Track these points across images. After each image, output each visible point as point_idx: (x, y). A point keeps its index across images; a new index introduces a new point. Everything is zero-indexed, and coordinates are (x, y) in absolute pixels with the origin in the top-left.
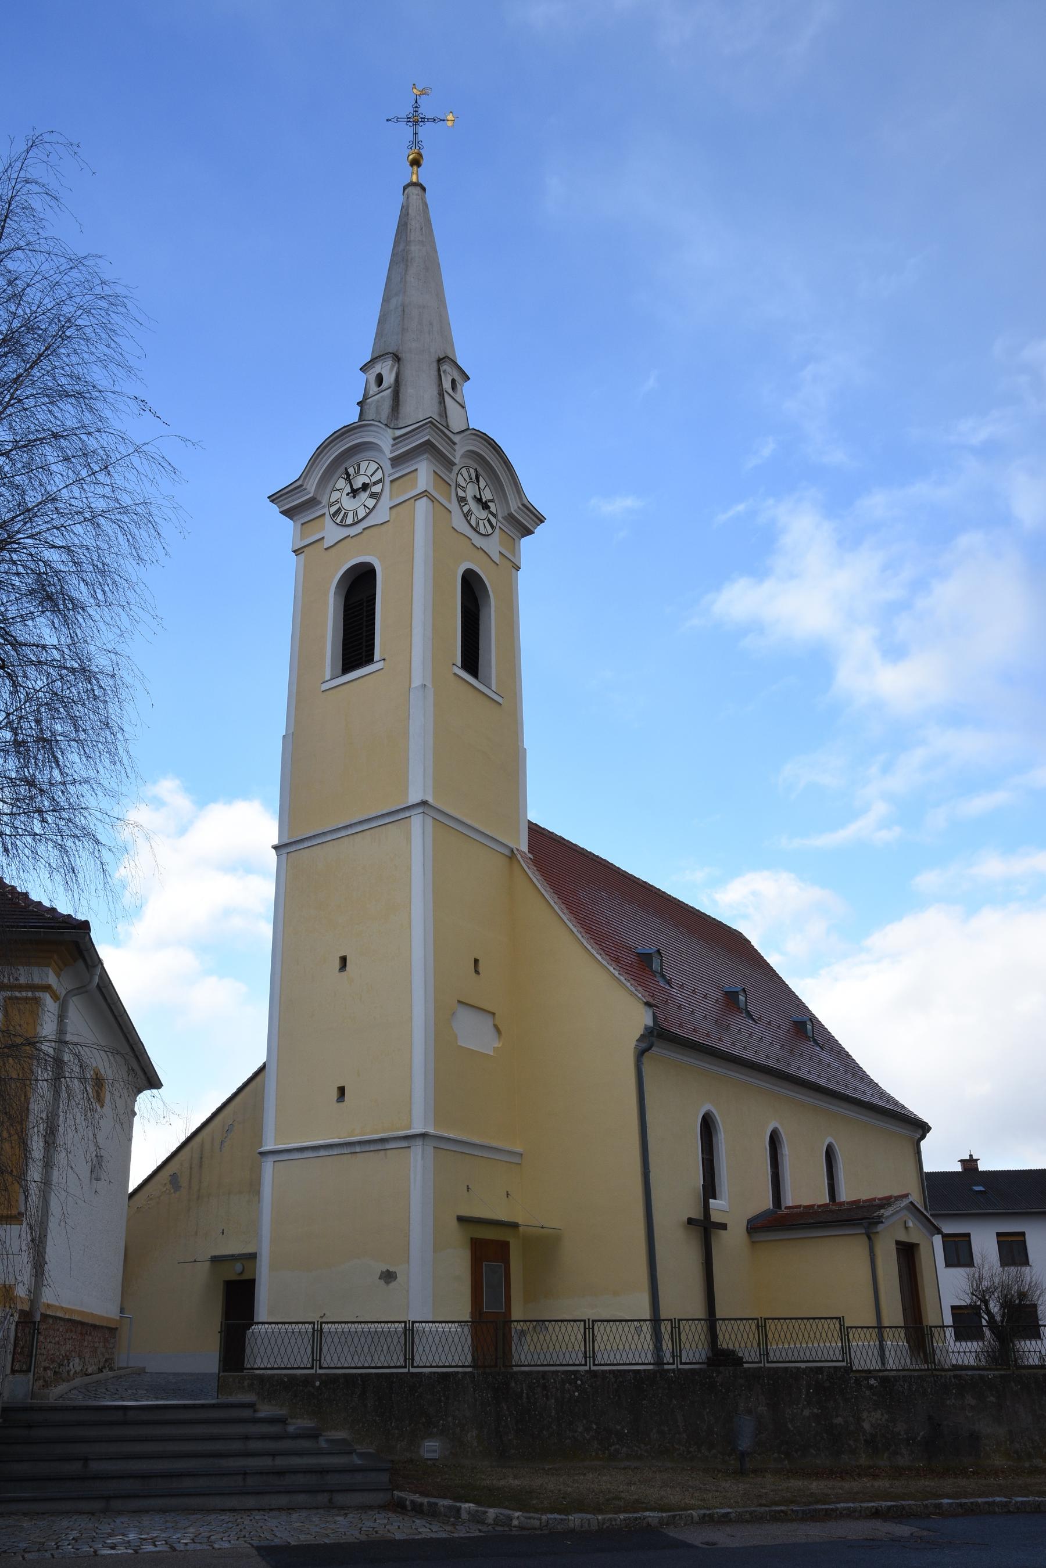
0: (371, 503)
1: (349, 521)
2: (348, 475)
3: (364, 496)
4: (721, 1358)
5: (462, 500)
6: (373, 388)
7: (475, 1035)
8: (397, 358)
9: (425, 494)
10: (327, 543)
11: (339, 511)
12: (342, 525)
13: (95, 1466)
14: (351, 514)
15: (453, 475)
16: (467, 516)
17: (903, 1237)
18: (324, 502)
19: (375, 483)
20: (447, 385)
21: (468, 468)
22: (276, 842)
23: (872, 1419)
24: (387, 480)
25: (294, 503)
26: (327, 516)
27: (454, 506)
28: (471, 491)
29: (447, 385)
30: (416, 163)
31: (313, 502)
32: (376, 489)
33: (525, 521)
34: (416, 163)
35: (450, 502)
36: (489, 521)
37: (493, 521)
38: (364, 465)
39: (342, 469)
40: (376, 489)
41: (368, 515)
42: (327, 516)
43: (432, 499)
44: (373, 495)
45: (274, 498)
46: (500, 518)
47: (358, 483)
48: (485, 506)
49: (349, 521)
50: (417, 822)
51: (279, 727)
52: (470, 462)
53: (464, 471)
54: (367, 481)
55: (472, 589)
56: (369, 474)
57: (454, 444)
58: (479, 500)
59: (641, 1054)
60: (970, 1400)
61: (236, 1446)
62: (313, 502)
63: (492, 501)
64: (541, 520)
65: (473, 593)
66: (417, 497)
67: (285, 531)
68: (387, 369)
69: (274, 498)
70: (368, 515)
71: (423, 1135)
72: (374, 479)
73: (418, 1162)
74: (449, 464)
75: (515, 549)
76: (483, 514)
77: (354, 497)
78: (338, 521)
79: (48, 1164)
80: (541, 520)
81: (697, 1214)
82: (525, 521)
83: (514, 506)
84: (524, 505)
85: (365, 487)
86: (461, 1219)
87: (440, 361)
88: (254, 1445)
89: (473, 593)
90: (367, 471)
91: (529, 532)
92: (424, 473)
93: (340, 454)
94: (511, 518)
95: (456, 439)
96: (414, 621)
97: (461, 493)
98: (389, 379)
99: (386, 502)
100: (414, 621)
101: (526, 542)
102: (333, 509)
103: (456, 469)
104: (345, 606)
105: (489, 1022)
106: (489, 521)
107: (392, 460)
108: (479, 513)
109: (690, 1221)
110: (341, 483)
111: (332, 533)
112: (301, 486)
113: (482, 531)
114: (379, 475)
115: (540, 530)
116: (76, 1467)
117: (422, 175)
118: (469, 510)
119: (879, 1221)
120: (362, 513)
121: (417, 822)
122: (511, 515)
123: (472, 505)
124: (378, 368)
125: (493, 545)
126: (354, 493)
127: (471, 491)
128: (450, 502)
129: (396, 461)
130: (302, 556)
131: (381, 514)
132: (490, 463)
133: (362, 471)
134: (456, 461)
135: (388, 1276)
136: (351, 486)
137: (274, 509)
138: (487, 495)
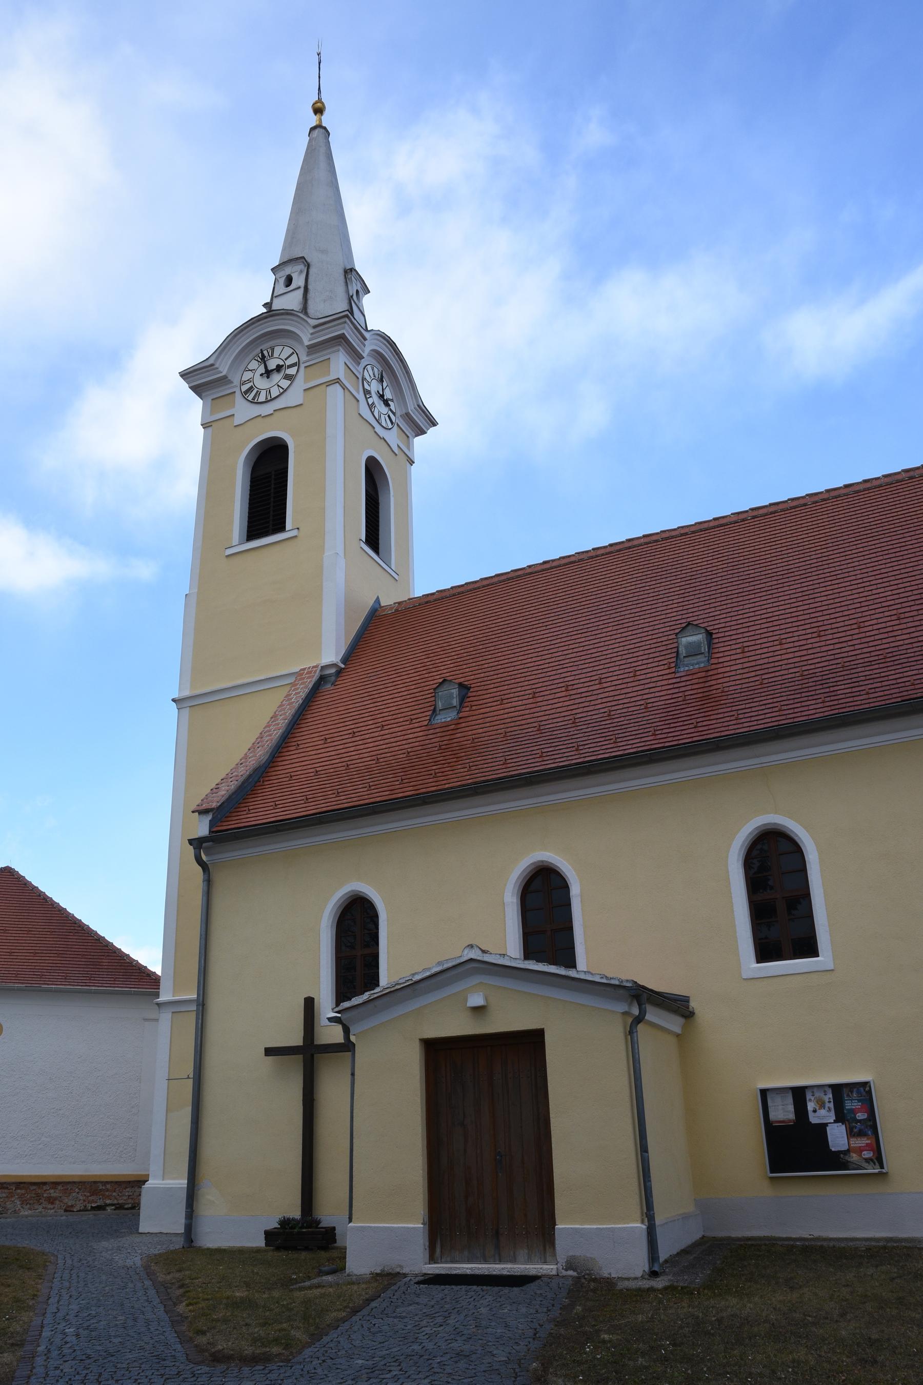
0: (285, 383)
1: (262, 398)
2: (263, 356)
3: (277, 377)
5: (367, 393)
6: (281, 289)
10: (237, 420)
11: (250, 389)
14: (263, 394)
16: (371, 407)
18: (236, 382)
19: (290, 366)
24: (302, 366)
26: (238, 395)
28: (374, 387)
32: (292, 371)
35: (358, 392)
36: (389, 416)
38: (277, 350)
39: (258, 350)
40: (292, 371)
41: (281, 394)
42: (238, 395)
43: (344, 388)
44: (288, 377)
45: (185, 375)
46: (398, 414)
47: (272, 364)
48: (386, 403)
49: (262, 398)
52: (374, 362)
53: (369, 367)
54: (281, 363)
55: (374, 474)
56: (283, 356)
57: (365, 339)
58: (381, 396)
63: (392, 400)
64: (434, 423)
66: (329, 384)
67: (196, 405)
70: (281, 394)
72: (288, 362)
74: (357, 356)
75: (409, 445)
76: (384, 410)
77: (268, 377)
78: (250, 398)
79: (628, 1279)
80: (434, 423)
82: (420, 421)
84: (419, 406)
85: (279, 368)
90: (281, 354)
91: (423, 432)
92: (339, 363)
93: (258, 338)
94: (408, 417)
96: (325, 496)
99: (300, 383)
102: (244, 388)
103: (363, 363)
104: (252, 478)
106: (389, 416)
107: (309, 347)
108: (381, 408)
112: (212, 365)
113: (384, 424)
114: (294, 359)
115: (432, 431)
118: (373, 403)
120: (275, 392)
122: (408, 414)
123: (375, 399)
124: (288, 270)
126: (268, 373)
128: (358, 392)
129: (312, 349)
130: (210, 429)
131: (295, 395)
132: (390, 364)
133: (276, 355)
134: (365, 355)
136: (266, 367)
137: (184, 385)
138: (388, 395)
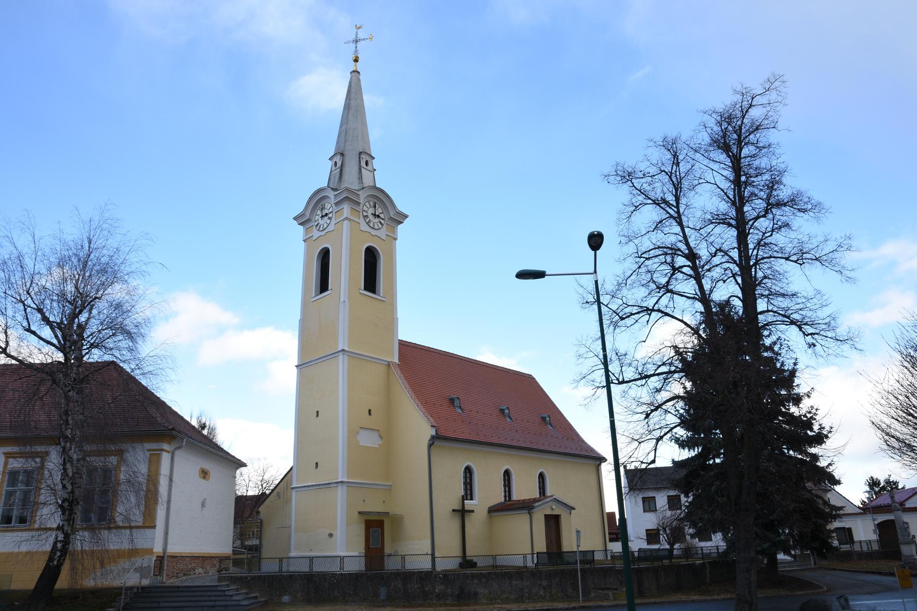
0: (328, 221)
3: (326, 218)
4: (467, 563)
7: (368, 440)
8: (342, 154)
9: (346, 218)
12: (319, 230)
13: (162, 605)
15: (361, 207)
17: (549, 512)
20: (363, 164)
21: (369, 202)
22: (296, 364)
23: (439, 588)
25: (303, 220)
27: (362, 220)
29: (363, 164)
30: (356, 60)
31: (309, 220)
32: (330, 215)
33: (399, 218)
34: (356, 60)
37: (382, 221)
43: (350, 220)
44: (330, 218)
45: (295, 219)
50: (341, 356)
51: (298, 316)
58: (375, 215)
59: (430, 446)
60: (476, 581)
61: (207, 598)
62: (309, 220)
64: (406, 216)
65: (371, 256)
68: (338, 159)
69: (295, 219)
71: (342, 482)
73: (341, 492)
74: (358, 204)
75: (394, 231)
76: (377, 220)
80: (406, 216)
81: (457, 506)
83: (392, 214)
85: (326, 214)
86: (360, 513)
87: (360, 153)
88: (212, 598)
89: (371, 256)
93: (317, 200)
94: (391, 219)
95: (360, 193)
97: (365, 214)
98: (339, 164)
99: (333, 222)
100: (347, 271)
101: (400, 226)
105: (376, 434)
109: (454, 510)
110: (319, 212)
111: (316, 234)
116: (156, 605)
117: (360, 66)
119: (533, 508)
121: (341, 356)
123: (371, 217)
124: (335, 160)
125: (382, 233)
127: (371, 211)
132: (380, 198)
135: (331, 535)
